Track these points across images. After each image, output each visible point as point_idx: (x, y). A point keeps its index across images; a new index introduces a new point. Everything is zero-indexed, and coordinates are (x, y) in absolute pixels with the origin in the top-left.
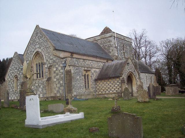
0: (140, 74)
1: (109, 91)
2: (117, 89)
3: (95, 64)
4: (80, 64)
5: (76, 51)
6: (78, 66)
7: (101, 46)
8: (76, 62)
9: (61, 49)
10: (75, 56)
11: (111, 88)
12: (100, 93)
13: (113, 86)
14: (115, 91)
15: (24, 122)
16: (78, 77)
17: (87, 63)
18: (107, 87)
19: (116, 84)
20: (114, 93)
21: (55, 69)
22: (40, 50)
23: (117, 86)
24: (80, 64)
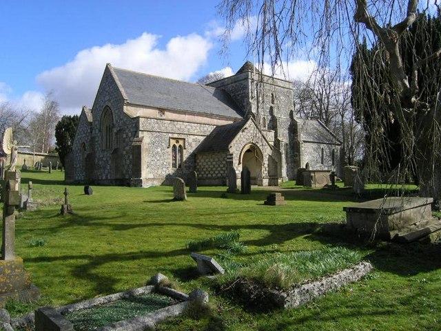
0: (303, 145)
1: (212, 175)
2: (222, 172)
3: (196, 129)
4: (163, 128)
5: (170, 107)
6: (159, 132)
7: (232, 95)
8: (157, 125)
9: (148, 105)
10: (168, 115)
11: (214, 169)
12: (210, 175)
13: (217, 166)
14: (219, 175)
15: (342, 226)
16: (159, 150)
17: (178, 126)
18: (224, 171)
19: (222, 163)
20: (218, 178)
21: (125, 136)
22: (110, 105)
23: (222, 166)
24: (163, 128)
